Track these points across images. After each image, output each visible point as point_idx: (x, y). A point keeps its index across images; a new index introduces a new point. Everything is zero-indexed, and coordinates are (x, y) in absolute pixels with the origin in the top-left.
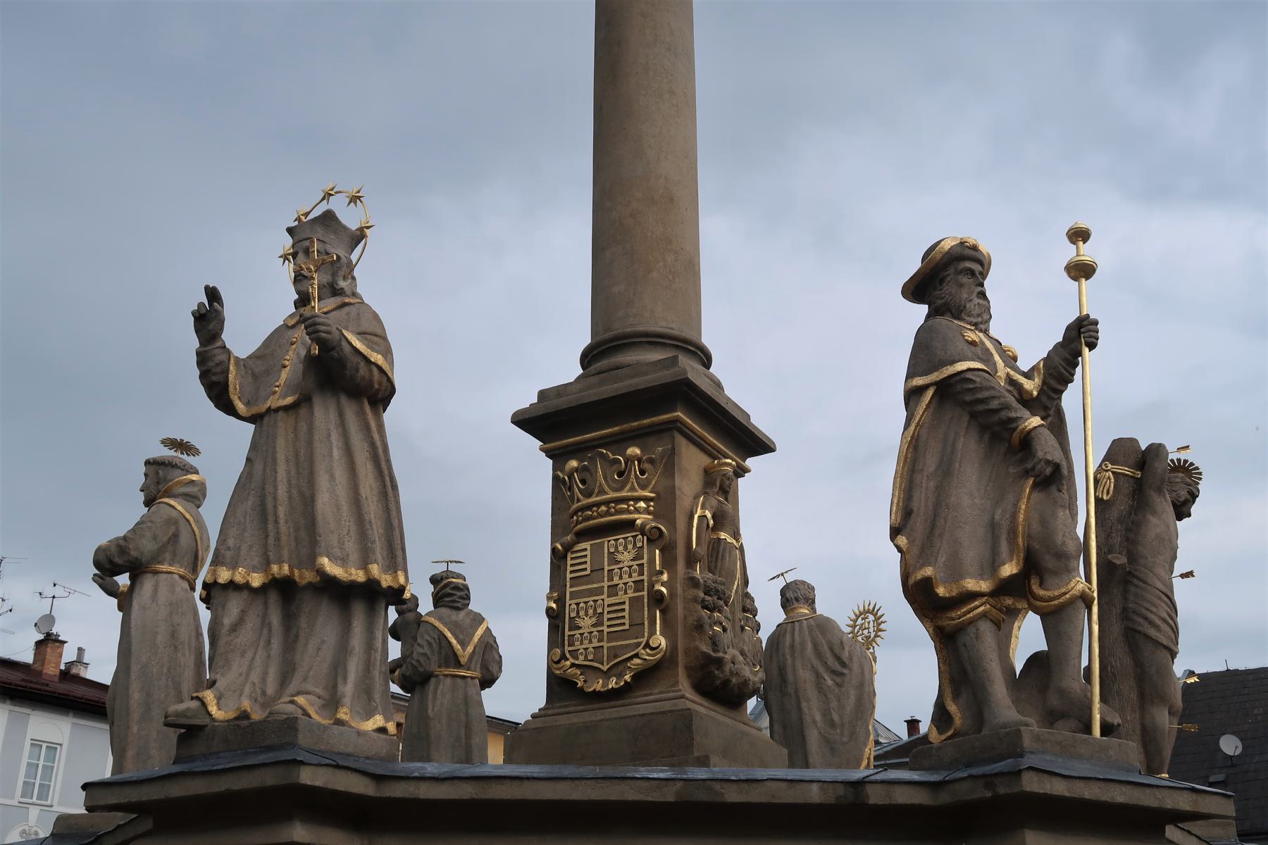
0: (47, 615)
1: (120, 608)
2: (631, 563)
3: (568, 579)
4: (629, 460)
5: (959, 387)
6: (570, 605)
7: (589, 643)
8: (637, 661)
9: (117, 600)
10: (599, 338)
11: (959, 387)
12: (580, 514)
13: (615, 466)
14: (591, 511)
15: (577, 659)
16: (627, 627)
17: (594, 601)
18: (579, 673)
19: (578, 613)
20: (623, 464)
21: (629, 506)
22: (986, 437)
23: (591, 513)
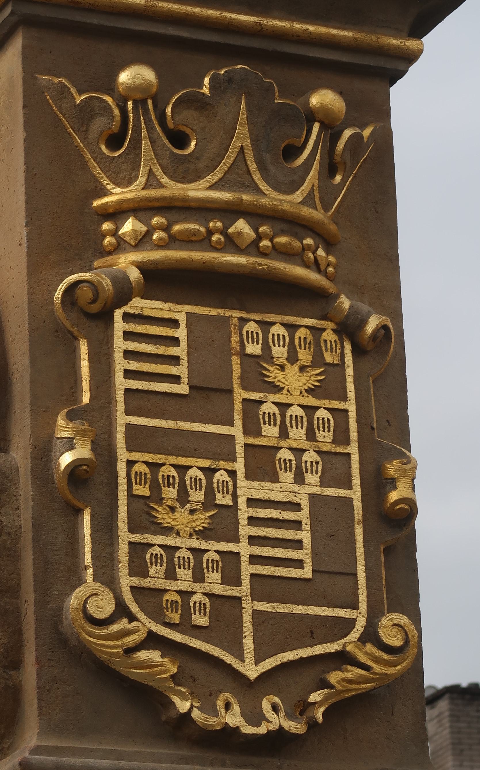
16: (183, 389)
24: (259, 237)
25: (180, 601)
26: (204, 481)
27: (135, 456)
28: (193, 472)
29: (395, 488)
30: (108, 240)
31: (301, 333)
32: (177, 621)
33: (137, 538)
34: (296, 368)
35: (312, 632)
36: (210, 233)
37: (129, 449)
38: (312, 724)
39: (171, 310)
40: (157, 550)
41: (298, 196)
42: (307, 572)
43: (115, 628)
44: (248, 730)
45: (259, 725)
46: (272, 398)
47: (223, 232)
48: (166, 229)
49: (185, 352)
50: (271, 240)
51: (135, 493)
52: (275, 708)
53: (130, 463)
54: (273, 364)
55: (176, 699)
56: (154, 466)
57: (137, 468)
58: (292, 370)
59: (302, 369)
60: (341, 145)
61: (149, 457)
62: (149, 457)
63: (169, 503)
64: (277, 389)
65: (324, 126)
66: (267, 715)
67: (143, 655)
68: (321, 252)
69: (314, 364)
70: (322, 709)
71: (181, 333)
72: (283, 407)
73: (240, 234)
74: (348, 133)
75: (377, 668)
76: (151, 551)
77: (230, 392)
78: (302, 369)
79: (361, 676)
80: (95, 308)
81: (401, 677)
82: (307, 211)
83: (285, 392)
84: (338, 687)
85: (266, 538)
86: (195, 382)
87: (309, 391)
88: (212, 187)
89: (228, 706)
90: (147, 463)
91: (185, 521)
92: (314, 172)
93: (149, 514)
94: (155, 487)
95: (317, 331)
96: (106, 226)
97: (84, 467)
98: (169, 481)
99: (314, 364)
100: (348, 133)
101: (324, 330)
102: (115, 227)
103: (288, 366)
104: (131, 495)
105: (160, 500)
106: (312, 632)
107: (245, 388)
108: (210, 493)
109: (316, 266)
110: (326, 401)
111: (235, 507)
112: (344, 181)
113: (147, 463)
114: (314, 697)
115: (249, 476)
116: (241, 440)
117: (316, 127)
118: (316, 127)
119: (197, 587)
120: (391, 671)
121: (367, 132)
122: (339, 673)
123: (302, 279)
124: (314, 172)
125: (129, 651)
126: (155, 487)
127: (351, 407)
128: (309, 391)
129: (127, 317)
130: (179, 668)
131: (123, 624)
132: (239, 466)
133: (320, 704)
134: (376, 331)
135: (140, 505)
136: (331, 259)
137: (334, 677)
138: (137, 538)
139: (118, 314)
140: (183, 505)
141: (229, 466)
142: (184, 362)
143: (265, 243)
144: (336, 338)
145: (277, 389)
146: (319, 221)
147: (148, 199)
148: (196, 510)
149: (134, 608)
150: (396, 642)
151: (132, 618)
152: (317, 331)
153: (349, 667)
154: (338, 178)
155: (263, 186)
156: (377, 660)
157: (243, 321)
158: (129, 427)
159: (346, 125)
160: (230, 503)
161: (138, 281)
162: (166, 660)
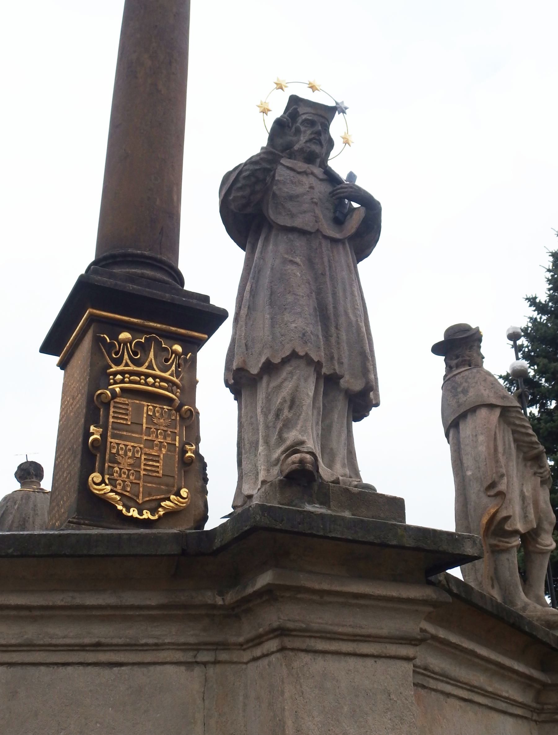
0: (26, 462)
1: (236, 399)
2: (165, 429)
3: (110, 424)
4: (173, 352)
5: (514, 414)
7: (127, 478)
8: (168, 503)
9: (211, 303)
10: (101, 256)
11: (514, 414)
12: (127, 375)
13: (163, 353)
14: (140, 378)
15: (116, 487)
16: (161, 475)
17: (132, 446)
18: (119, 499)
19: (118, 451)
20: (117, 346)
21: (141, 379)
22: (521, 456)
23: (139, 379)
24: (155, 382)
26: (116, 447)
27: (113, 440)
28: (129, 447)
29: (188, 453)
30: (112, 381)
33: (110, 464)
42: (161, 475)
51: (112, 452)
56: (118, 444)
61: (132, 444)
62: (132, 444)
92: (174, 366)
96: (111, 377)
98: (122, 449)
99: (168, 419)
102: (150, 384)
108: (133, 453)
117: (174, 356)
119: (119, 478)
123: (129, 387)
124: (174, 366)
135: (112, 455)
138: (110, 464)
139: (112, 402)
143: (157, 384)
147: (169, 378)
148: (522, 491)
159: (133, 340)
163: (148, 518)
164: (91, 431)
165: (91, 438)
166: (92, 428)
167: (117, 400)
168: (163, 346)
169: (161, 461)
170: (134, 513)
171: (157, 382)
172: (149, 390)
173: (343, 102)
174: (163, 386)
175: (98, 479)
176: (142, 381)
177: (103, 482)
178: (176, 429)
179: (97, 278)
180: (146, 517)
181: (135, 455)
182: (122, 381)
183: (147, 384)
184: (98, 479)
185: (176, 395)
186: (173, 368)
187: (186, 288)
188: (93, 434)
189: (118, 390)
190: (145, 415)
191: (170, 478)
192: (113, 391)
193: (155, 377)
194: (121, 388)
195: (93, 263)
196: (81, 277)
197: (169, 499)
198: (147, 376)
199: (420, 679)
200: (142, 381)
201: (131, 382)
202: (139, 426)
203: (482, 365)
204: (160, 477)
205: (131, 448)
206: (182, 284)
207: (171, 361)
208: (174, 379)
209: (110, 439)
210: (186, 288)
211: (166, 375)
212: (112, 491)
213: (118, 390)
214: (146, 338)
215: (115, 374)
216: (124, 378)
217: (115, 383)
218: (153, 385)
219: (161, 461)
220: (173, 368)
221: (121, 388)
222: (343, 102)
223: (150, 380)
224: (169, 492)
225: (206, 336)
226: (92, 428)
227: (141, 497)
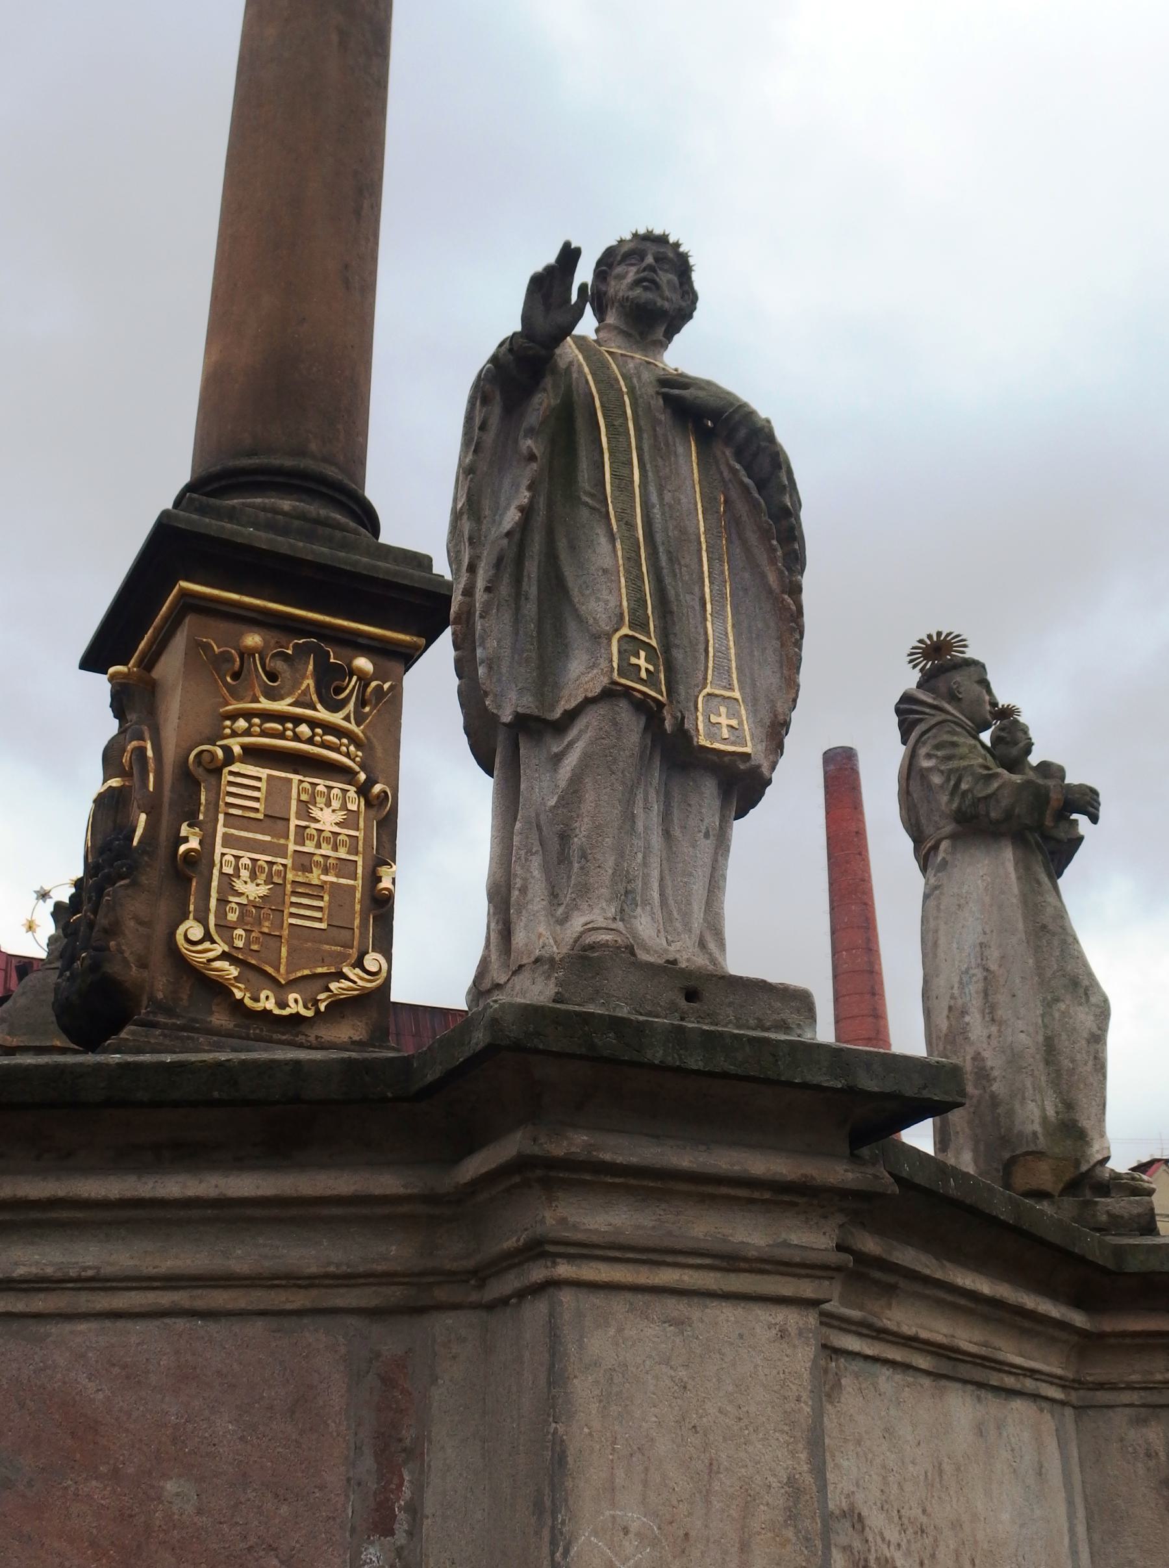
6: (223, 855)
16: (260, 816)
24: (314, 735)
25: (244, 936)
26: (233, 863)
27: (225, 850)
31: (335, 791)
32: (241, 946)
34: (330, 810)
35: (323, 959)
36: (285, 730)
37: (223, 846)
38: (318, 1011)
39: (258, 772)
40: (234, 905)
41: (342, 714)
43: (200, 947)
44: (277, 1011)
45: (284, 1008)
46: (313, 825)
47: (293, 731)
48: (260, 726)
49: (264, 796)
50: (321, 737)
51: (224, 871)
52: (296, 1001)
53: (223, 855)
54: (315, 806)
55: (235, 991)
56: (237, 858)
57: (226, 857)
58: (328, 811)
59: (334, 811)
60: (369, 690)
61: (269, 858)
63: (244, 879)
64: (317, 821)
65: (359, 679)
66: (290, 1004)
67: (217, 964)
68: (352, 748)
69: (341, 809)
70: (325, 1004)
71: (262, 785)
72: (320, 831)
73: (302, 732)
74: (374, 684)
75: (360, 983)
76: (230, 905)
77: (288, 820)
78: (334, 811)
79: (351, 987)
80: (212, 766)
81: (378, 988)
82: (345, 724)
83: (321, 823)
84: (335, 992)
85: (301, 904)
86: (266, 813)
87: (336, 824)
88: (289, 705)
89: (267, 998)
90: (233, 856)
91: (253, 889)
93: (231, 884)
94: (237, 869)
95: (345, 791)
96: (228, 723)
97: (193, 854)
99: (341, 809)
100: (374, 684)
101: (349, 791)
103: (325, 809)
104: (221, 873)
105: (239, 877)
106: (323, 959)
107: (298, 818)
109: (348, 755)
110: (346, 830)
111: (284, 885)
112: (371, 711)
113: (233, 856)
114: (321, 996)
115: (294, 868)
116: (292, 847)
117: (355, 678)
118: (355, 678)
120: (369, 985)
121: (386, 686)
122: (337, 983)
125: (210, 961)
126: (237, 869)
127: (360, 834)
128: (336, 824)
129: (231, 773)
130: (239, 973)
131: (207, 945)
132: (288, 862)
133: (323, 1000)
134: (379, 794)
136: (360, 754)
137: (333, 986)
139: (226, 770)
140: (252, 882)
141: (283, 861)
142: (263, 801)
144: (356, 796)
145: (317, 821)
146: (1137, 1424)
149: (216, 937)
150: (374, 969)
151: (213, 942)
152: (345, 791)
153: (343, 981)
154: (367, 709)
155: (319, 706)
156: (361, 979)
157: (301, 781)
158: (225, 835)
160: (281, 882)
161: (239, 755)
162: (232, 967)
163: (298, 1013)
164: (183, 833)
165: (182, 848)
166: (184, 830)
167: (235, 768)
168: (332, 660)
169: (326, 898)
170: (267, 1002)
171: (255, 725)
172: (328, 758)
173: (42, 888)
174: (329, 741)
175: (197, 932)
176: (289, 733)
177: (207, 937)
178: (290, 781)
179: (194, 520)
180: (294, 1011)
181: (272, 877)
182: (247, 733)
183: (297, 738)
184: (197, 932)
185: (353, 760)
186: (351, 706)
187: (385, 538)
188: (186, 840)
189: (237, 750)
190: (294, 804)
191: (343, 931)
192: (227, 750)
193: (313, 723)
194: (244, 747)
195: (189, 488)
196: (165, 514)
197: (341, 976)
198: (297, 720)
199: (825, 1319)
200: (289, 733)
201: (264, 734)
202: (280, 822)
203: (464, 717)
204: (260, 820)
205: (265, 865)
206: (375, 529)
207: (347, 691)
208: (352, 726)
209: (219, 849)
210: (385, 538)
211: (336, 718)
212: (224, 956)
213: (237, 750)
214: (296, 646)
215: (233, 717)
216: (251, 725)
217: (234, 734)
218: (310, 741)
219: (326, 898)
220: (351, 706)
221: (244, 747)
222: (42, 888)
223: (304, 729)
224: (343, 958)
225: (423, 641)
226: (184, 830)
227: (283, 969)
